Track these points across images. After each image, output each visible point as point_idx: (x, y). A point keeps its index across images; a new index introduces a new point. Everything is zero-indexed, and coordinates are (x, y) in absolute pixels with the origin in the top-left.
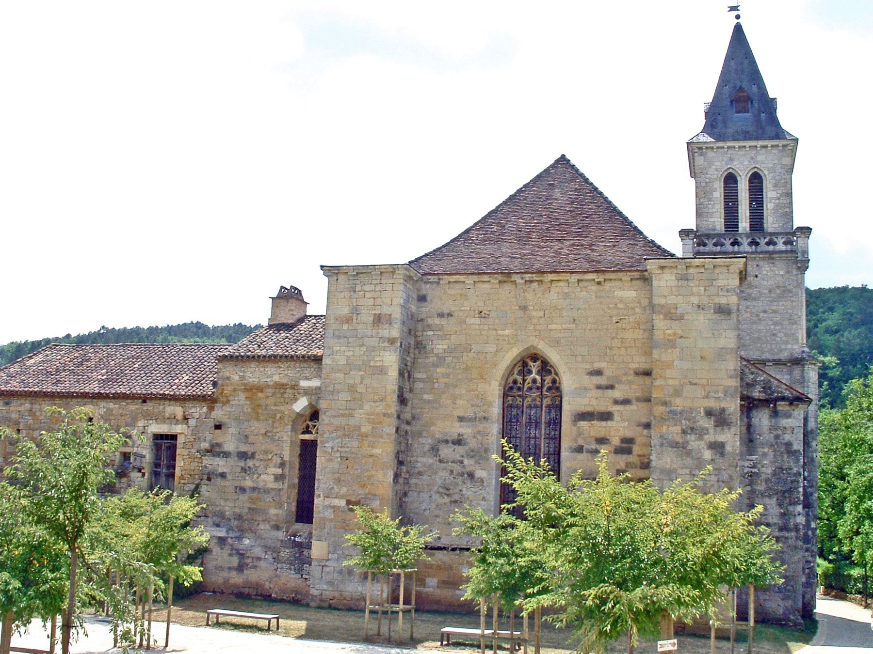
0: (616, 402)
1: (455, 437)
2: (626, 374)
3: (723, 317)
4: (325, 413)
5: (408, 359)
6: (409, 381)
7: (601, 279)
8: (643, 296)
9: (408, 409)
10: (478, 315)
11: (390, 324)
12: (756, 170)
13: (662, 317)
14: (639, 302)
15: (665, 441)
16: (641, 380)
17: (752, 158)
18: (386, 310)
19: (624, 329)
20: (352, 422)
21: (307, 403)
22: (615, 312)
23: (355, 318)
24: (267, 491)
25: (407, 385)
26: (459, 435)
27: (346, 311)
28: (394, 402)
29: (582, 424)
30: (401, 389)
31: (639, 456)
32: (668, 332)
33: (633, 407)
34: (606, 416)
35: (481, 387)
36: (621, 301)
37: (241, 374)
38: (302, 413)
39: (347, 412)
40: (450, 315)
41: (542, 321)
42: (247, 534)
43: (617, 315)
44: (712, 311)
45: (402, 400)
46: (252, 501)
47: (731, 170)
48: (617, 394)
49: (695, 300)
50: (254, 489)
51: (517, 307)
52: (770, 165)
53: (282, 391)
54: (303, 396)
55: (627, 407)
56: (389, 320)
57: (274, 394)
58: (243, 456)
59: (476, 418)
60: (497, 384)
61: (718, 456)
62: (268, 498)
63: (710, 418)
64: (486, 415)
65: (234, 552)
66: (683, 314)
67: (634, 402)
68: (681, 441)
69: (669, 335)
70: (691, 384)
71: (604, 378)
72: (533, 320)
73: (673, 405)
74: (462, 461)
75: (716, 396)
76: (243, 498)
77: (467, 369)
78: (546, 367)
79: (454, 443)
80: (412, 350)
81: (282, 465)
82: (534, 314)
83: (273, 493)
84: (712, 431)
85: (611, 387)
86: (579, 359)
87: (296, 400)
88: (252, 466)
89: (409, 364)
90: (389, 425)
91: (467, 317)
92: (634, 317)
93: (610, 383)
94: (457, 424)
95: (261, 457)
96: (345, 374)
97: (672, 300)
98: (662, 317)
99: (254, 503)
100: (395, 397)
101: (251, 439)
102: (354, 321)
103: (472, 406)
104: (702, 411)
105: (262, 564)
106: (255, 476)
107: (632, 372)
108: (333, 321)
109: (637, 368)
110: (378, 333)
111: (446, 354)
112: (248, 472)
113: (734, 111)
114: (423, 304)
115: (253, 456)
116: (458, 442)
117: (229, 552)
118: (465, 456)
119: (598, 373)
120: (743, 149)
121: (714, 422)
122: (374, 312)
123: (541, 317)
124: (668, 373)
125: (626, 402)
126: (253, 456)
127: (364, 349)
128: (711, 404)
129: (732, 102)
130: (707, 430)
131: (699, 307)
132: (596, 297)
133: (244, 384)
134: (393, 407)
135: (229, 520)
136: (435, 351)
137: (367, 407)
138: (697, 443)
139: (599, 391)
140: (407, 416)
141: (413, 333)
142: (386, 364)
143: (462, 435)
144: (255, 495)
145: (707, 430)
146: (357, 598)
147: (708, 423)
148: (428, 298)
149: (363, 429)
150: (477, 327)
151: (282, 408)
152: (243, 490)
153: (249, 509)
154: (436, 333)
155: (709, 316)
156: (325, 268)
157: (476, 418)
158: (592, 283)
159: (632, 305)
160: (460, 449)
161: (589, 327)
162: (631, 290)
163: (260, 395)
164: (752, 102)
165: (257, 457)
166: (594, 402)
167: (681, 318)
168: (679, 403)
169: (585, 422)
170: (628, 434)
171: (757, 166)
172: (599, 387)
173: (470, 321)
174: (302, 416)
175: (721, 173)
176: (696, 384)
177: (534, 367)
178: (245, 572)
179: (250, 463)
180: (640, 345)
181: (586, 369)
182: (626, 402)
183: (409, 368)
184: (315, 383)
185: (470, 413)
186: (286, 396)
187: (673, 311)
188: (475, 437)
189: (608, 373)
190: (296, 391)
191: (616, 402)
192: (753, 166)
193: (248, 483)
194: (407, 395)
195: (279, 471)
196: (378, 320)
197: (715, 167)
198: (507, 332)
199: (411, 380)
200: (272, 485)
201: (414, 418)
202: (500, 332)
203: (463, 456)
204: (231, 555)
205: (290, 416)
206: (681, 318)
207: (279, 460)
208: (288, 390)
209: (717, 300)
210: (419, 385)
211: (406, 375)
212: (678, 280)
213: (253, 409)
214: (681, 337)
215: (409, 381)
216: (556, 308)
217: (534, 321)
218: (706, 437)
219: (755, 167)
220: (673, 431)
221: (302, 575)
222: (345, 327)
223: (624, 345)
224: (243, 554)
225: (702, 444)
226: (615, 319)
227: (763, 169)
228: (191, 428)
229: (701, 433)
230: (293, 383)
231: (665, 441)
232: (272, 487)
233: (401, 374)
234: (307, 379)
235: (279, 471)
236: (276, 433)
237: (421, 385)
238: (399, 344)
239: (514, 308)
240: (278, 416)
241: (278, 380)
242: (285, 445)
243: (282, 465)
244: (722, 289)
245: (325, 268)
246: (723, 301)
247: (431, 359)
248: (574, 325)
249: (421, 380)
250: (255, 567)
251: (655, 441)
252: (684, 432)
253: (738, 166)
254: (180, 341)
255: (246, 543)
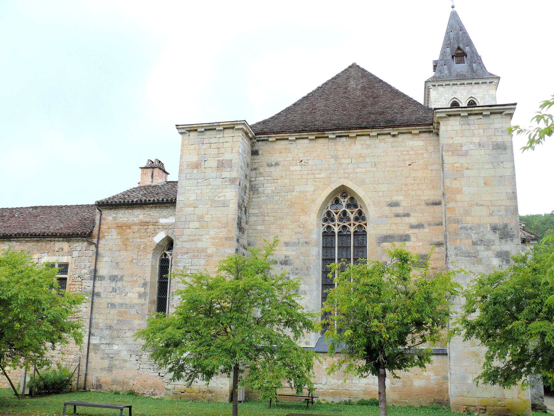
0: (412, 227)
1: (282, 258)
2: (418, 205)
3: (500, 152)
4: (178, 239)
5: (245, 197)
6: (246, 214)
7: (396, 133)
8: (429, 144)
9: (245, 236)
10: (299, 164)
11: (231, 167)
12: (472, 99)
13: (450, 153)
14: (427, 150)
15: (459, 252)
16: (431, 208)
17: (469, 91)
18: (227, 156)
19: (416, 170)
20: (200, 245)
21: (165, 236)
22: (407, 157)
23: (203, 164)
24: (132, 306)
25: (244, 217)
26: (286, 256)
27: (194, 159)
28: (234, 228)
29: (385, 244)
30: (240, 219)
31: (433, 268)
32: (456, 165)
33: (427, 230)
34: (405, 238)
35: (303, 218)
36: (412, 149)
37: (114, 215)
38: (161, 244)
39: (196, 237)
40: (277, 164)
41: (350, 166)
42: (116, 342)
43: (410, 159)
44: (491, 148)
45: (241, 229)
46: (120, 314)
47: (455, 100)
48: (413, 220)
49: (476, 140)
50: (121, 305)
51: (330, 157)
52: (481, 95)
53: (146, 227)
54: (162, 231)
55: (421, 230)
56: (230, 164)
57: (139, 229)
58: (113, 278)
59: (299, 243)
60: (316, 216)
61: (504, 263)
62: (133, 311)
63: (495, 232)
64: (307, 240)
65: (106, 356)
66: (468, 151)
67: (426, 226)
68: (472, 251)
69: (457, 167)
70: (477, 205)
71: (401, 208)
72: (343, 165)
73: (464, 222)
74: (289, 277)
75: (499, 214)
76: (113, 312)
77: (292, 205)
78: (353, 203)
79: (281, 263)
80: (247, 191)
81: (145, 285)
82: (343, 161)
83: (137, 308)
84: (497, 242)
85: (408, 215)
86: (381, 194)
87: (157, 234)
88: (121, 287)
89: (245, 201)
90: (230, 247)
91: (290, 165)
92: (423, 161)
93: (406, 212)
94: (284, 248)
95: (128, 279)
96: (195, 207)
97: (458, 140)
98: (450, 153)
99: (122, 316)
100: (235, 226)
101: (121, 265)
102: (202, 166)
103: (296, 233)
104: (488, 225)
105: (128, 365)
106: (123, 295)
107: (423, 203)
108: (185, 167)
109: (427, 200)
110: (221, 175)
111: (274, 194)
112: (118, 292)
113: (455, 62)
114: (256, 157)
115: (122, 279)
116: (285, 262)
117: (101, 356)
118: (291, 273)
119: (395, 204)
120: (463, 85)
121: (499, 235)
122: (218, 159)
123: (349, 163)
124: (458, 197)
125: (420, 226)
126: (122, 279)
127: (210, 187)
128: (496, 220)
129: (453, 57)
130: (494, 241)
131: (480, 145)
132: (392, 147)
133: (117, 223)
134: (235, 232)
135: (102, 329)
136: (266, 192)
137: (212, 233)
138: (486, 252)
139: (399, 218)
140: (244, 242)
141: (248, 178)
142: (227, 198)
143: (288, 257)
144: (123, 309)
145: (494, 241)
146: (204, 390)
147: (495, 237)
148: (260, 152)
149: (209, 251)
150: (298, 172)
151: (146, 240)
152: (113, 305)
153: (118, 320)
154: (266, 178)
155: (489, 152)
156: (179, 127)
157: (299, 243)
158: (389, 136)
159: (420, 152)
160: (287, 268)
161: (387, 169)
162: (419, 141)
163: (128, 231)
164: (466, 56)
165: (125, 279)
166: (394, 227)
167: (466, 154)
168: (469, 221)
169: (388, 243)
170: (423, 252)
171: (472, 96)
172: (397, 216)
173: (292, 168)
174: (162, 246)
175: (448, 101)
176: (481, 205)
177: (344, 202)
178: (114, 372)
179: (119, 284)
180: (429, 182)
181: (387, 202)
182: (420, 226)
183: (245, 205)
184: (171, 220)
185: (294, 239)
186: (148, 230)
187: (459, 148)
188: (298, 258)
189: (403, 204)
190: (156, 227)
191: (412, 227)
192: (470, 96)
193: (117, 300)
194: (243, 225)
195: (142, 290)
196: (221, 165)
197: (444, 97)
198: (322, 176)
199: (247, 214)
200: (137, 301)
201: (249, 244)
202: (317, 176)
203: (289, 274)
204: (102, 358)
205: (151, 247)
206: (466, 154)
207: (142, 281)
208: (151, 227)
209: (494, 139)
210: (252, 219)
211: (243, 209)
212: (462, 125)
213: (123, 242)
214: (467, 169)
215: (246, 214)
216: (360, 156)
217: (344, 166)
218: (493, 247)
219: (471, 97)
220: (465, 244)
221: (159, 373)
222: (195, 171)
223: (416, 182)
224: (112, 358)
225: (490, 253)
226: (408, 163)
227: (477, 98)
228: (74, 259)
229: (488, 245)
230: (154, 221)
231: (459, 252)
232: (136, 303)
233: (240, 207)
234: (165, 217)
235: (142, 290)
236: (140, 260)
237: (255, 218)
238: (238, 183)
239: (327, 157)
240: (142, 246)
241: (142, 219)
242: (147, 269)
243: (145, 285)
244: (497, 131)
245: (179, 127)
246: (499, 139)
247: (263, 198)
248: (375, 169)
249: (255, 215)
250: (121, 368)
251: (451, 252)
252: (474, 244)
253: (460, 97)
254: (217, 384)
255: (115, 348)
